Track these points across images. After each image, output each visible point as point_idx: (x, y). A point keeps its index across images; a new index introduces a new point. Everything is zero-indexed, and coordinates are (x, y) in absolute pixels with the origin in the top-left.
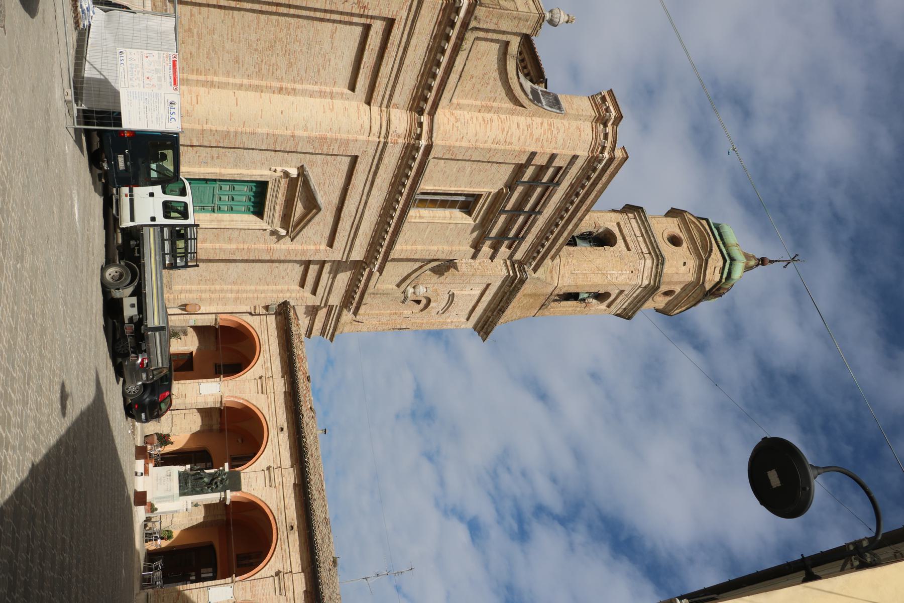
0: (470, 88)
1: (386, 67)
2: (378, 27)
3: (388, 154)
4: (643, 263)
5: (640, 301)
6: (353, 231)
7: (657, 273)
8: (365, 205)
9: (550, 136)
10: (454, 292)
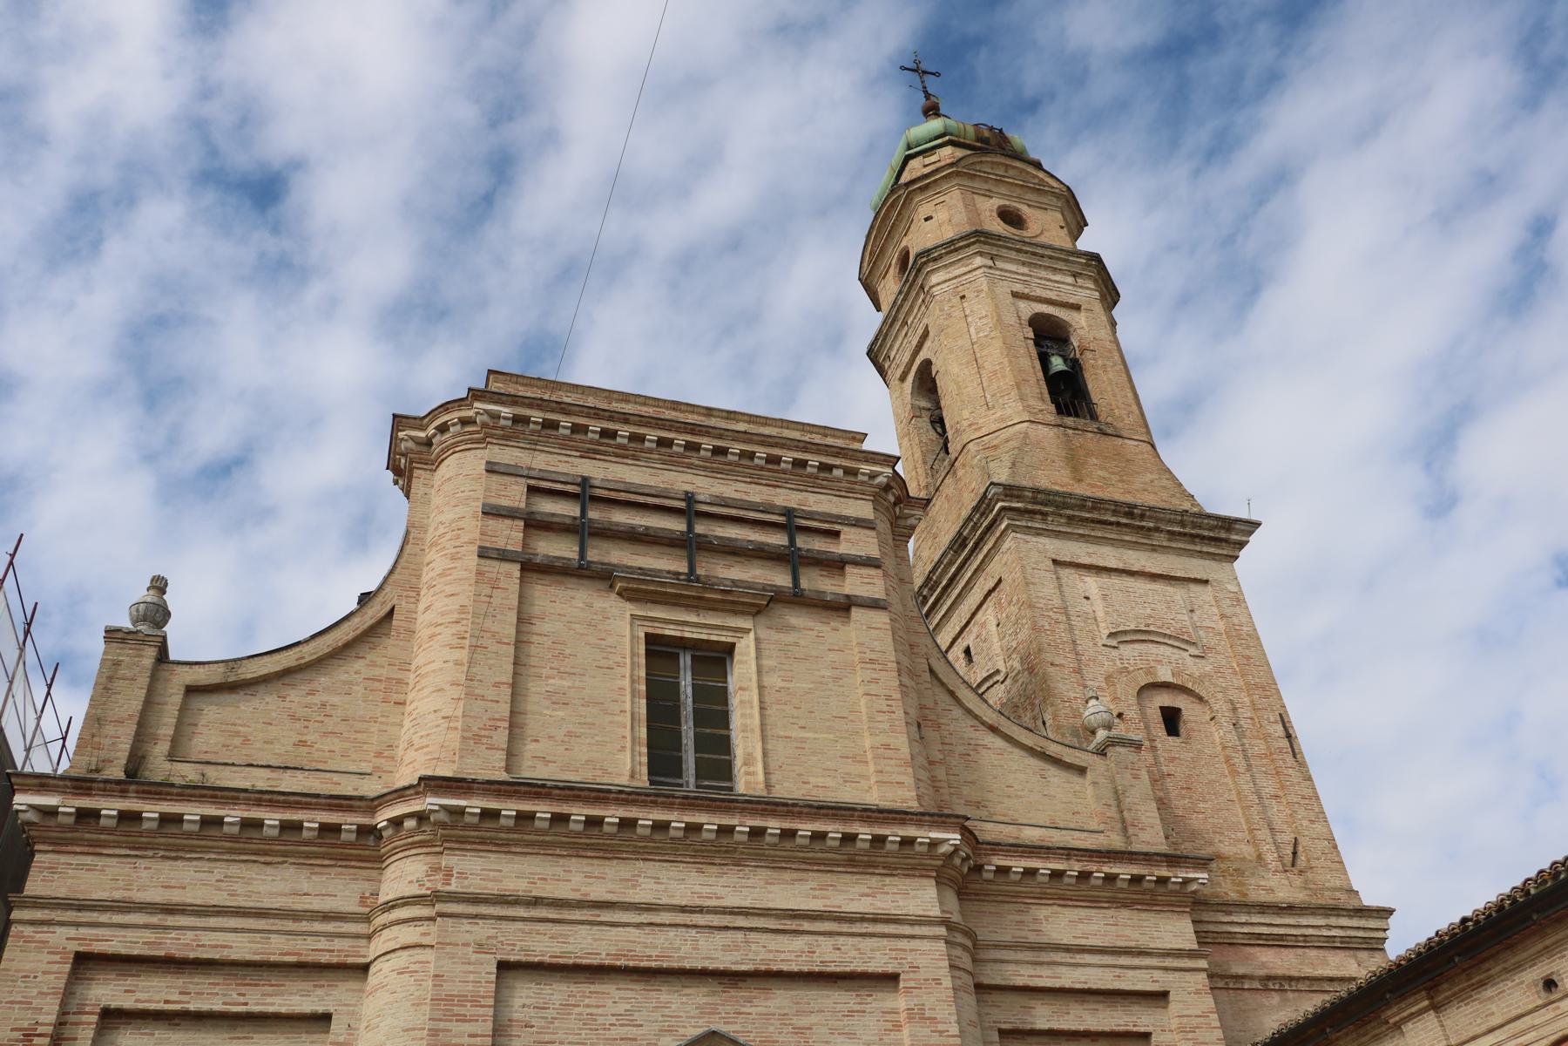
0: (336, 740)
1: (231, 947)
2: (108, 991)
3: (490, 885)
4: (939, 287)
5: (1034, 254)
6: (806, 926)
7: (951, 252)
8: (692, 912)
9: (448, 536)
10: (1105, 637)
